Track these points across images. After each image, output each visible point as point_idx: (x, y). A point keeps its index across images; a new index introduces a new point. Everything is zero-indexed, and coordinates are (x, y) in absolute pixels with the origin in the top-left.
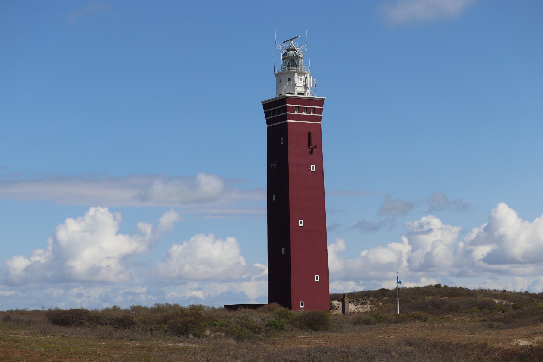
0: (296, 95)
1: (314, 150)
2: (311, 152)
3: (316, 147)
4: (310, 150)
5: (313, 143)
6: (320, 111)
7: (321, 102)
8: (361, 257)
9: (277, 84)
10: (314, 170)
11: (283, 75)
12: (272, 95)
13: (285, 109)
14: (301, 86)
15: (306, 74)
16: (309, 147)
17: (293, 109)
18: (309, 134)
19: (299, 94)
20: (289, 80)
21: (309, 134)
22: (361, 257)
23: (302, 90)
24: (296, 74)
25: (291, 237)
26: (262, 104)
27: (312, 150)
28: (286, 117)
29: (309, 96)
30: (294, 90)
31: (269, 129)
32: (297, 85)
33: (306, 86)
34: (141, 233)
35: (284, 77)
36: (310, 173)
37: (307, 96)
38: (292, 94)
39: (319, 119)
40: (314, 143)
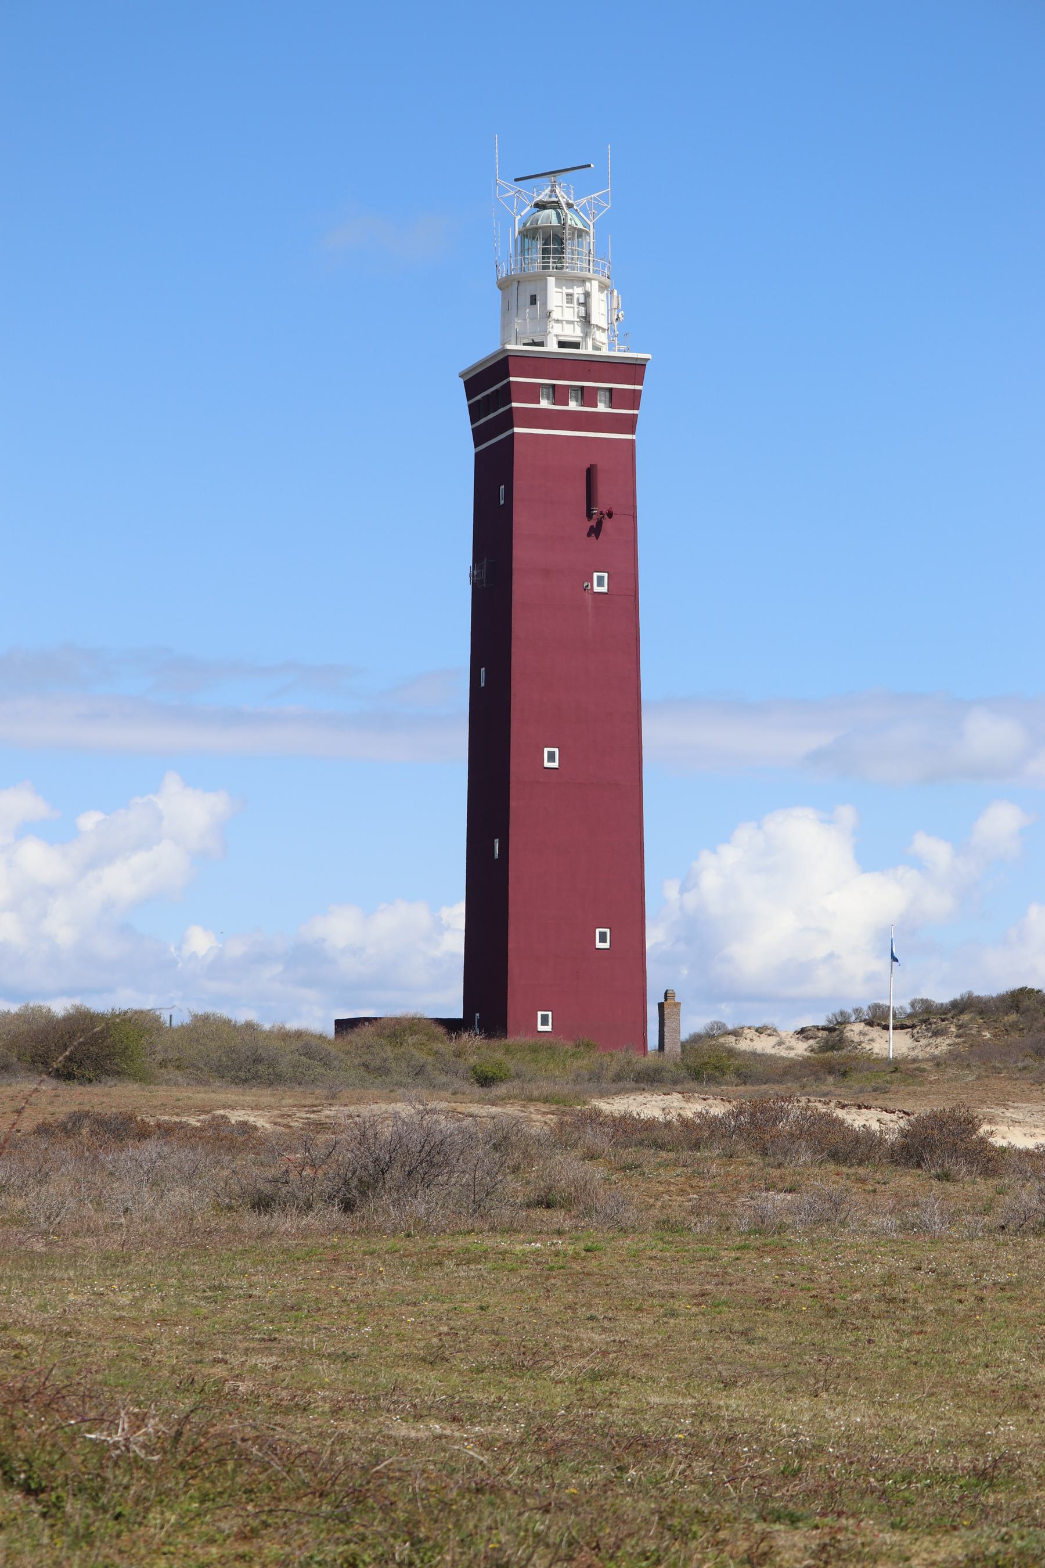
0: (552, 346)
1: (607, 523)
2: (595, 531)
3: (610, 515)
4: (593, 523)
5: (603, 504)
6: (633, 399)
7: (634, 370)
8: (782, 899)
9: (503, 316)
10: (604, 589)
11: (515, 284)
12: (479, 352)
13: (506, 395)
14: (579, 315)
15: (590, 280)
16: (589, 515)
17: (532, 393)
18: (590, 474)
19: (562, 344)
20: (533, 300)
21: (590, 474)
22: (782, 899)
23: (573, 333)
24: (551, 281)
25: (513, 804)
26: (461, 382)
27: (600, 523)
28: (508, 420)
29: (605, 352)
30: (546, 333)
31: (478, 456)
32: (555, 315)
33: (586, 320)
34: (918, 863)
35: (521, 293)
36: (589, 597)
37: (590, 351)
38: (541, 344)
39: (629, 424)
40: (603, 502)
